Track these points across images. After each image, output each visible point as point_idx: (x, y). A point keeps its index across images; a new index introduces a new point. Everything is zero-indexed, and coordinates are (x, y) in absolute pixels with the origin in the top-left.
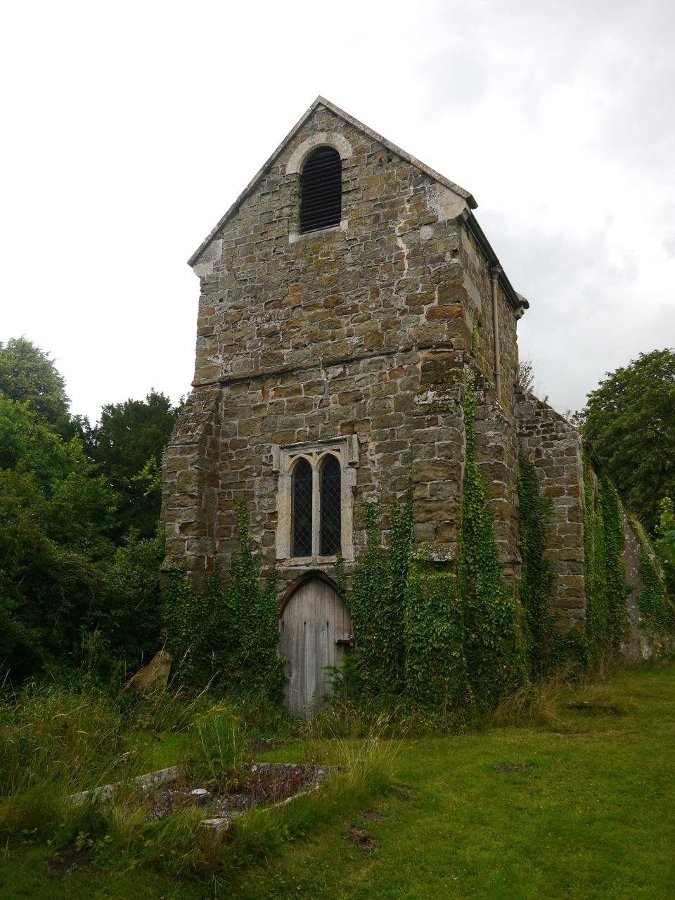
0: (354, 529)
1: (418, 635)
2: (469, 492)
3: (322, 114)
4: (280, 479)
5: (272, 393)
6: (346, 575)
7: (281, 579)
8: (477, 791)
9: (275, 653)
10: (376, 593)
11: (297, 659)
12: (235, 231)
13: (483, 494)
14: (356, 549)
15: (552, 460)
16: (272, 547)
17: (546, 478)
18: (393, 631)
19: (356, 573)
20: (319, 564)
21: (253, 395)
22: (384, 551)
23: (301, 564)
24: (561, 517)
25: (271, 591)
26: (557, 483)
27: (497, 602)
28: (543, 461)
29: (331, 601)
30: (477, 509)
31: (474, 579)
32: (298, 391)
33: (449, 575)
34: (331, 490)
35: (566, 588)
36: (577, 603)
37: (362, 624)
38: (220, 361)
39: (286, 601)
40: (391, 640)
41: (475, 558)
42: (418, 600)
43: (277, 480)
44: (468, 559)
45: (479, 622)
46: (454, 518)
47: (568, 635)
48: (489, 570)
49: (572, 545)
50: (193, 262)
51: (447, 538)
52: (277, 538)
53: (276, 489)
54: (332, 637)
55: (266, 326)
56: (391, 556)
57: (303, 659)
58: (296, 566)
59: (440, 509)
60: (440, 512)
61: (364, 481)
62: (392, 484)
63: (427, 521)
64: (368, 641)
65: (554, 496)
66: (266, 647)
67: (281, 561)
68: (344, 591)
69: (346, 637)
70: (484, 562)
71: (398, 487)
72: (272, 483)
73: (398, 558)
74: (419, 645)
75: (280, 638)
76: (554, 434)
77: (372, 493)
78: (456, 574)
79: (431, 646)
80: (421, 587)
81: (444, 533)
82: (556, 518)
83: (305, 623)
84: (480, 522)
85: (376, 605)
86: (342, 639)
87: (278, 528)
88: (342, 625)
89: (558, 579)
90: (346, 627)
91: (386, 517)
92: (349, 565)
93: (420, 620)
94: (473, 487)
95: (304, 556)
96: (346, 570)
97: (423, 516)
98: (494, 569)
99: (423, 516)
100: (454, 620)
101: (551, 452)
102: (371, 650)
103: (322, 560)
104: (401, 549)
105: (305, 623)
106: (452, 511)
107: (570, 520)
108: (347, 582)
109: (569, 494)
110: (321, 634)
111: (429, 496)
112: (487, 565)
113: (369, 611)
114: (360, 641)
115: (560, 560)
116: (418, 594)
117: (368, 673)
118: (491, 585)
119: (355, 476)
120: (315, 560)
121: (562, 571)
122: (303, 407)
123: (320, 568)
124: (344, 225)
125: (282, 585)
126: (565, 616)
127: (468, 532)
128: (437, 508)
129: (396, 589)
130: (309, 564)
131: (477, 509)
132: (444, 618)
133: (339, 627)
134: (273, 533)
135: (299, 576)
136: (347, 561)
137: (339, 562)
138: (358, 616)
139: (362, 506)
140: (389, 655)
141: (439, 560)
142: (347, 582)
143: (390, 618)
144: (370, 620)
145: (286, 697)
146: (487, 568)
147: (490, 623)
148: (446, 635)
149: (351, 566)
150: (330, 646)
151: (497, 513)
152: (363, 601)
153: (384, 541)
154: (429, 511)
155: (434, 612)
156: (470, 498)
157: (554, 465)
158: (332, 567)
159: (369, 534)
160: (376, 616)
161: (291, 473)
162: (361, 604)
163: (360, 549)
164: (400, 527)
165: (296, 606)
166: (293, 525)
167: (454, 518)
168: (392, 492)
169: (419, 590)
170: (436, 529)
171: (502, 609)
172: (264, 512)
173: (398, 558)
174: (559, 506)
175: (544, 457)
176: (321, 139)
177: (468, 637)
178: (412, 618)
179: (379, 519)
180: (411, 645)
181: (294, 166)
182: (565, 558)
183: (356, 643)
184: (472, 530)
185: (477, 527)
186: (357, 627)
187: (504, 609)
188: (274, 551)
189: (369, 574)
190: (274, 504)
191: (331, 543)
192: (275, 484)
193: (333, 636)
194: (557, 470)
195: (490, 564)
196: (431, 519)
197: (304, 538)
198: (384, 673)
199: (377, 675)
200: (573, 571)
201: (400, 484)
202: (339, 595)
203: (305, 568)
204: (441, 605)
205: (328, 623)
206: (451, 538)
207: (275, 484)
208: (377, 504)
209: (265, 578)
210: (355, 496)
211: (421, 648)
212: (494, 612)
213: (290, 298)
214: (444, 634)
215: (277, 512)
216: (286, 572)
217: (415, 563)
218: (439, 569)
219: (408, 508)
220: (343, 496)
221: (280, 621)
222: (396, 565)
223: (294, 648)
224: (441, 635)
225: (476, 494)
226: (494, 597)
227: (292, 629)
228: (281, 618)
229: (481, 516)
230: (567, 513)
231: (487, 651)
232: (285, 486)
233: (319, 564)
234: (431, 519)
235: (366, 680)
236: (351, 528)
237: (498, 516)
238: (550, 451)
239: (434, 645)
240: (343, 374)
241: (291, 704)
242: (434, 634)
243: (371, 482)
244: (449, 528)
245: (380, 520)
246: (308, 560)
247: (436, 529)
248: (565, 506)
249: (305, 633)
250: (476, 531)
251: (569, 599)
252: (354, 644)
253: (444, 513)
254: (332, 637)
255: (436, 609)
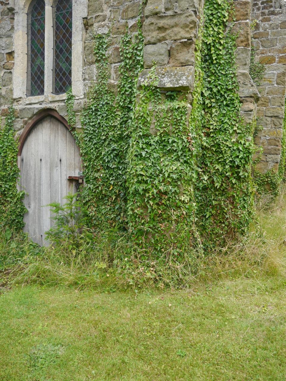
0: (85, 64)
1: (142, 175)
2: (210, 12)
4: (16, 18)
6: (75, 112)
7: (18, 117)
8: (148, 8)
9: (14, 187)
10: (103, 131)
11: (35, 192)
13: (226, 14)
14: (85, 85)
15: (268, 32)
16: (9, 87)
17: (261, 48)
18: (120, 170)
19: (85, 109)
20: (51, 102)
22: (113, 86)
23: (38, 102)
24: (270, 81)
25: (9, 130)
26: (270, 53)
27: (234, 140)
28: (260, 34)
29: (64, 138)
30: (219, 33)
31: (209, 115)
33: (183, 104)
34: (64, 26)
35: (268, 139)
36: (276, 150)
37: (90, 161)
39: (24, 139)
40: (117, 178)
41: (211, 91)
42: (143, 135)
43: (13, 19)
44: (204, 92)
45: (211, 163)
46: (193, 35)
47: (266, 174)
48: (227, 105)
49: (277, 104)
51: (183, 61)
52: (14, 78)
53: (13, 28)
54: (64, 173)
56: (120, 91)
57: (40, 193)
58: (30, 104)
59: (176, 25)
60: (176, 29)
61: (95, 12)
62: (124, 11)
63: (160, 41)
64: (96, 179)
65: (266, 64)
66: (6, 182)
67: (17, 100)
68: (74, 129)
69: (76, 174)
70: (222, 95)
71: (130, 14)
72: (9, 22)
73: (127, 93)
74: (141, 187)
75: (19, 173)
76: (272, 9)
77: (103, 23)
78: (191, 104)
79: (157, 187)
80: (149, 119)
81: (179, 55)
82: (266, 82)
83: (41, 160)
84: (221, 48)
85: (103, 143)
86: (73, 175)
87: (14, 67)
88: (73, 162)
89: (263, 131)
90: (77, 164)
91: (117, 49)
92: (79, 101)
93: (145, 159)
94: (215, 6)
95: (39, 94)
96: (75, 107)
97: (155, 35)
98: (233, 104)
99: (155, 35)
100: (185, 159)
101: (268, 26)
102: (98, 187)
103: (53, 97)
104: (131, 82)
105: (41, 160)
106: (192, 26)
107: (277, 84)
108: (77, 119)
109: (280, 62)
110: (55, 171)
111: (163, 10)
112: (225, 98)
113: (97, 148)
114: (88, 178)
115: (266, 116)
116: (145, 128)
117: (94, 209)
118: (228, 121)
119: (86, 5)
120: (48, 98)
121: (267, 124)
123: (52, 106)
125: (19, 124)
126: (265, 160)
127: (206, 61)
128: (172, 24)
129: (124, 126)
130: (42, 102)
131: (219, 33)
132: (174, 156)
133: (71, 164)
134: (11, 72)
135: (34, 115)
136: (77, 98)
137: (69, 99)
138: (86, 154)
139: (92, 39)
140: (115, 193)
141: (171, 86)
142: (77, 119)
143: (117, 155)
144: (97, 157)
145: (26, 226)
146: (225, 103)
147: (224, 164)
148: (175, 176)
149: (80, 103)
150: (63, 182)
151: (242, 38)
152: (91, 138)
153: (113, 75)
154: (161, 29)
155: (162, 149)
156: (211, 20)
157: (269, 37)
158: (63, 104)
159: (98, 68)
160: (103, 153)
161: (26, 11)
162: (89, 141)
163: (89, 85)
164: (130, 58)
165: (33, 143)
166: (30, 64)
167: (193, 35)
168: (124, 21)
169: (145, 123)
170: (169, 51)
171: (238, 149)
172: (3, 52)
173: (127, 93)
174: (270, 72)
175: (261, 30)
177: (199, 180)
178: (136, 156)
179: (110, 51)
180: (134, 187)
182: (270, 115)
183: (85, 180)
184: (211, 58)
185: (218, 55)
186: (85, 165)
187: (241, 149)
188: (11, 90)
189: (96, 110)
190: (11, 44)
191: (63, 81)
192: (12, 23)
193: (65, 173)
194: (271, 41)
195: (228, 98)
196: (164, 39)
197: (39, 78)
198: (110, 209)
199: (103, 212)
200: (276, 125)
201: (132, 10)
202: (70, 132)
203: (38, 106)
204: (170, 141)
205: (60, 160)
206: (188, 60)
207: (12, 23)
208: (108, 35)
209: (5, 117)
210: (87, 29)
211: (146, 191)
212: (229, 152)
214: (171, 175)
215: (13, 52)
216: (22, 110)
217: (142, 91)
218: (171, 98)
219: (140, 37)
220: (74, 30)
221: (19, 158)
222: (125, 100)
223: (32, 182)
224: (168, 177)
225: (219, 14)
226: (231, 135)
227: (30, 165)
228: (20, 155)
229: (222, 42)
230: (276, 78)
231: (217, 193)
232: (21, 23)
233: (51, 102)
234: (164, 39)
235: (92, 217)
236: (81, 63)
237: (242, 42)
238: (267, 24)
239: (160, 188)
241: (30, 231)
242: (161, 175)
243: (102, 11)
244: (186, 50)
245: (110, 52)
246: (41, 98)
247: (169, 51)
248: (275, 72)
249: (41, 169)
250: (216, 59)
251: (270, 147)
252: (83, 180)
253: (181, 30)
254: (64, 173)
255: (165, 146)
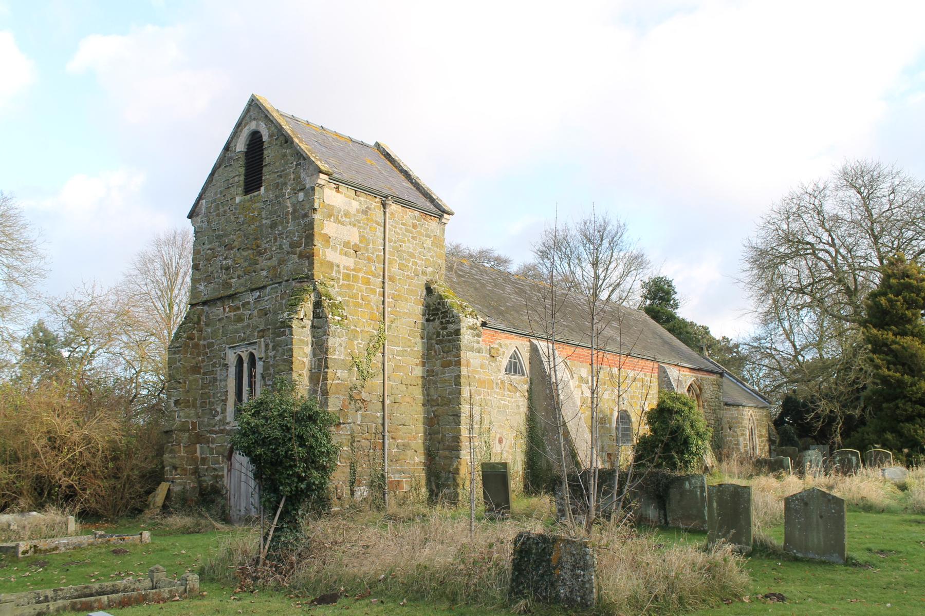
3: (255, 108)
5: (227, 309)
12: (210, 194)
21: (218, 311)
32: (239, 308)
38: (202, 288)
50: (190, 217)
55: (224, 263)
67: (228, 423)
122: (240, 319)
124: (262, 189)
176: (253, 126)
181: (241, 146)
213: (236, 243)
240: (259, 297)
